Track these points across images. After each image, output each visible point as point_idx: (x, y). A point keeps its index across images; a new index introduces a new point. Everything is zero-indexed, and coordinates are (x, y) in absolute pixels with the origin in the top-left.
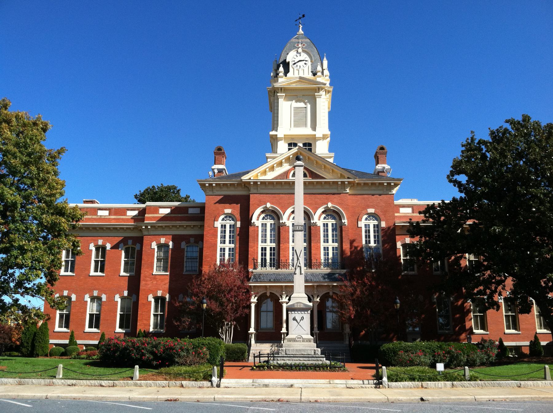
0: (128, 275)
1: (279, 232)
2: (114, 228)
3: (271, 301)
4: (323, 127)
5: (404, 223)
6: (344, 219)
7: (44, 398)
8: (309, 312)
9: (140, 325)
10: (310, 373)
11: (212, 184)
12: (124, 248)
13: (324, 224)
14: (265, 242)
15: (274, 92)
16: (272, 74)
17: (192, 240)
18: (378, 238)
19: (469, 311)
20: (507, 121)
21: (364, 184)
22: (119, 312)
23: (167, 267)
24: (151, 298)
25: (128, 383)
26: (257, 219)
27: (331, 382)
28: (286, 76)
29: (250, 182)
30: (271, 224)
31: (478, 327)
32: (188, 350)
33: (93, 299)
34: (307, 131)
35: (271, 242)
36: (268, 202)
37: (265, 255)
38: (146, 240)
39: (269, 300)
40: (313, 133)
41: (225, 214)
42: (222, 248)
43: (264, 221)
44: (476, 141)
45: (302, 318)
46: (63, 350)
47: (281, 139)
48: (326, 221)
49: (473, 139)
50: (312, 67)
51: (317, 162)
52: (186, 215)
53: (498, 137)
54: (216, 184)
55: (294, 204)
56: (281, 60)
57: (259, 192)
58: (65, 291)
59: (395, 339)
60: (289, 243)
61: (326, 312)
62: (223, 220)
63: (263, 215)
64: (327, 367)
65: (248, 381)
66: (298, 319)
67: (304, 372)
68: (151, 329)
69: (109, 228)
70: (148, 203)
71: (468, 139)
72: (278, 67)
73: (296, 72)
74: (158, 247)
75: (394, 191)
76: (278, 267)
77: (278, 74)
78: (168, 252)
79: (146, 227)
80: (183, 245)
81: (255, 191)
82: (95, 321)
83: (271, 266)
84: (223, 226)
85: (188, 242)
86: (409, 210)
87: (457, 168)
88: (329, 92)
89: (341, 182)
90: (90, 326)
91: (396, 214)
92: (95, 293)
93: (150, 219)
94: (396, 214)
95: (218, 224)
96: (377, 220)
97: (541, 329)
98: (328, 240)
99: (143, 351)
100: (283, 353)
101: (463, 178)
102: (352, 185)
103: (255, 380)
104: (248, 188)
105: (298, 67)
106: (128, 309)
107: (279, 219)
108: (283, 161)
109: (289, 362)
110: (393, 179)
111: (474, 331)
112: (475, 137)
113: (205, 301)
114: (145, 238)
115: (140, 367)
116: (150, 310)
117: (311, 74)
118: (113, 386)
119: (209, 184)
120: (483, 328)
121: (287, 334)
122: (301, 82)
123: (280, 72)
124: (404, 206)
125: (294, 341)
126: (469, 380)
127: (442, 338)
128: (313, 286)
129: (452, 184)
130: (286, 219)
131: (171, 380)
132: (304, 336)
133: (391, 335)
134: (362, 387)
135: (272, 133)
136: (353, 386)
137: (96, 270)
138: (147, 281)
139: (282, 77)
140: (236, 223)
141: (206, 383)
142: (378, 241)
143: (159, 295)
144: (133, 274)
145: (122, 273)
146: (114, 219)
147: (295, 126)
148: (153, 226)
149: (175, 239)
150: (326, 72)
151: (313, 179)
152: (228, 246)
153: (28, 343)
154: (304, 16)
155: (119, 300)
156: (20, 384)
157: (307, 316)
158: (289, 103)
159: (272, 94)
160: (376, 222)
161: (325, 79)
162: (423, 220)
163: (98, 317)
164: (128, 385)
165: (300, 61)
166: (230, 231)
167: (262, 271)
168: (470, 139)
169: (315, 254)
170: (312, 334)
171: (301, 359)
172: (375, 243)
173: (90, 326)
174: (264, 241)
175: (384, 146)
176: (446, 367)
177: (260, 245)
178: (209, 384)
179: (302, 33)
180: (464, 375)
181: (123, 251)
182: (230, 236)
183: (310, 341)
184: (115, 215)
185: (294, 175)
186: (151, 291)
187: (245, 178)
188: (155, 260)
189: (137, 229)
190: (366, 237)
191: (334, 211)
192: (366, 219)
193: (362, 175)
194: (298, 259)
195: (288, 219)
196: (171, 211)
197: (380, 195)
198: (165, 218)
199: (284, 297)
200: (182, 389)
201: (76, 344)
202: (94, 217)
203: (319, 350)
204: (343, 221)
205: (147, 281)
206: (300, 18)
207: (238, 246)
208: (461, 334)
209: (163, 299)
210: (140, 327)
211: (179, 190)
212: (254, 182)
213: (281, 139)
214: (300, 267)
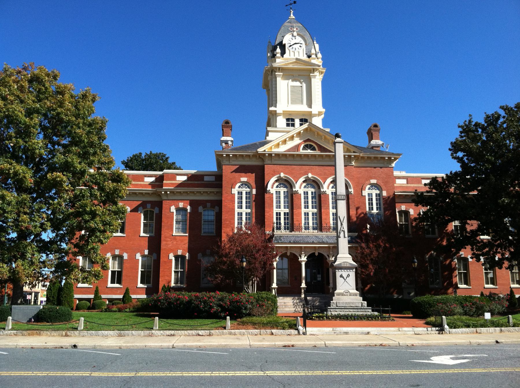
0: (148, 235)
1: (292, 199)
2: (133, 193)
4: (318, 106)
5: (401, 192)
6: (351, 188)
7: (171, 347)
8: (354, 270)
9: (162, 281)
10: (365, 322)
11: (229, 155)
12: (143, 211)
13: (304, 192)
14: (280, 208)
15: (273, 71)
16: (269, 54)
17: (209, 205)
18: (380, 205)
19: (455, 269)
20: (502, 108)
21: (368, 157)
22: (140, 269)
23: (186, 229)
24: (172, 257)
25: (223, 332)
26: (272, 187)
27: (400, 330)
28: (283, 57)
29: (265, 154)
30: (284, 192)
31: (462, 282)
32: (252, 303)
33: (114, 257)
34: (303, 108)
35: (285, 208)
36: (282, 172)
37: (280, 219)
38: (165, 204)
40: (309, 110)
41: (241, 182)
42: (239, 212)
43: (278, 189)
44: (473, 123)
45: (348, 276)
46: (88, 304)
47: (280, 115)
48: (306, 190)
49: (470, 121)
50: (306, 49)
51: (325, 138)
52: (203, 182)
53: (492, 120)
54: (233, 155)
56: (277, 42)
57: (273, 163)
59: (395, 293)
60: (301, 208)
61: (288, 269)
62: (239, 187)
63: (277, 184)
64: (378, 317)
65: (329, 329)
66: (345, 275)
67: (358, 321)
68: (173, 284)
69: (136, 193)
70: (166, 171)
71: (466, 121)
72: (275, 48)
73: (292, 54)
74: (176, 211)
75: (393, 165)
76: (292, 230)
77: (276, 55)
78: (186, 215)
79: (166, 192)
80: (200, 209)
81: (269, 162)
82: (117, 277)
83: (285, 229)
84: (240, 193)
85: (205, 207)
86: (404, 181)
87: (455, 147)
88: (322, 73)
89: (348, 155)
90: (113, 282)
92: (117, 252)
93: (168, 185)
95: (235, 191)
96: (379, 190)
97: (514, 284)
98: (280, 206)
99: (211, 304)
100: (335, 306)
101: (460, 154)
102: (357, 158)
103: (334, 328)
105: (294, 49)
106: (149, 267)
107: (319, 188)
108: (295, 135)
109: (342, 313)
110: (393, 154)
111: (459, 286)
112: (472, 120)
113: (244, 260)
114: (164, 203)
116: (171, 267)
117: (306, 56)
118: (210, 335)
119: (226, 155)
120: (466, 283)
122: (297, 63)
123: (277, 53)
124: (399, 178)
125: (343, 295)
126: (513, 326)
127: (433, 292)
128: (329, 247)
129: (456, 161)
130: (327, 188)
131: (260, 329)
132: (351, 291)
133: (392, 290)
134: (428, 334)
135: (271, 109)
136: (420, 333)
138: (167, 241)
139: (279, 58)
140: (252, 191)
141: (293, 332)
142: (380, 208)
143: (179, 254)
144: (153, 234)
145: (142, 234)
148: (172, 192)
149: (192, 203)
150: (320, 55)
152: (245, 210)
153: (53, 297)
154: (295, 2)
155: (140, 258)
156: (120, 335)
157: (352, 274)
158: (286, 82)
159: (270, 73)
160: (378, 192)
161: (318, 61)
162: (427, 191)
163: (120, 273)
164: (223, 334)
165: (296, 44)
166: (246, 197)
168: (468, 121)
169: (326, 219)
170: (357, 289)
171: (351, 310)
172: (377, 210)
173: (113, 282)
174: (279, 207)
175: (378, 124)
176: (492, 315)
177: (275, 210)
178: (296, 332)
179: (294, 17)
180: (509, 322)
181: (142, 214)
182: (246, 202)
183: (356, 295)
186: (171, 251)
187: (261, 150)
188: (175, 223)
189: (154, 194)
190: (369, 205)
191: (314, 181)
192: (369, 189)
193: (361, 149)
194: (342, 224)
195: (300, 188)
196: (188, 178)
197: (381, 168)
198: (182, 185)
199: (303, 256)
200: (272, 336)
201: (101, 299)
202: (142, 183)
203: (366, 302)
204: (350, 190)
205: (167, 241)
206: (291, 4)
207: (254, 211)
208: (448, 289)
209: (183, 257)
210: (162, 283)
211: (167, 158)
212: (269, 154)
213: (280, 115)
214: (344, 231)
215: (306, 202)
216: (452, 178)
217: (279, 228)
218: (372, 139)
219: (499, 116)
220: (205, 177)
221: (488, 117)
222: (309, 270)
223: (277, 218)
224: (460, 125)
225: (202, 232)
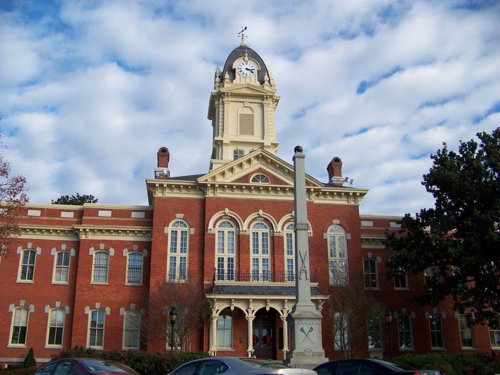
17: (135, 247)
20: (478, 135)
29: (206, 184)
40: (262, 141)
42: (176, 258)
49: (444, 150)
66: (306, 329)
71: (439, 150)
85: (97, 248)
95: (168, 230)
104: (204, 192)
129: (431, 194)
137: (23, 277)
146: (46, 220)
147: (241, 133)
151: (275, 184)
154: (246, 28)
157: (319, 322)
167: (253, 283)
168: (441, 150)
177: (217, 254)
184: (48, 215)
194: (303, 262)
215: (256, 245)
216: (426, 214)
217: (221, 277)
218: (333, 175)
219: (476, 144)
220: (133, 213)
221: (463, 145)
222: (257, 331)
223: (219, 265)
224: (433, 155)
225: (127, 281)
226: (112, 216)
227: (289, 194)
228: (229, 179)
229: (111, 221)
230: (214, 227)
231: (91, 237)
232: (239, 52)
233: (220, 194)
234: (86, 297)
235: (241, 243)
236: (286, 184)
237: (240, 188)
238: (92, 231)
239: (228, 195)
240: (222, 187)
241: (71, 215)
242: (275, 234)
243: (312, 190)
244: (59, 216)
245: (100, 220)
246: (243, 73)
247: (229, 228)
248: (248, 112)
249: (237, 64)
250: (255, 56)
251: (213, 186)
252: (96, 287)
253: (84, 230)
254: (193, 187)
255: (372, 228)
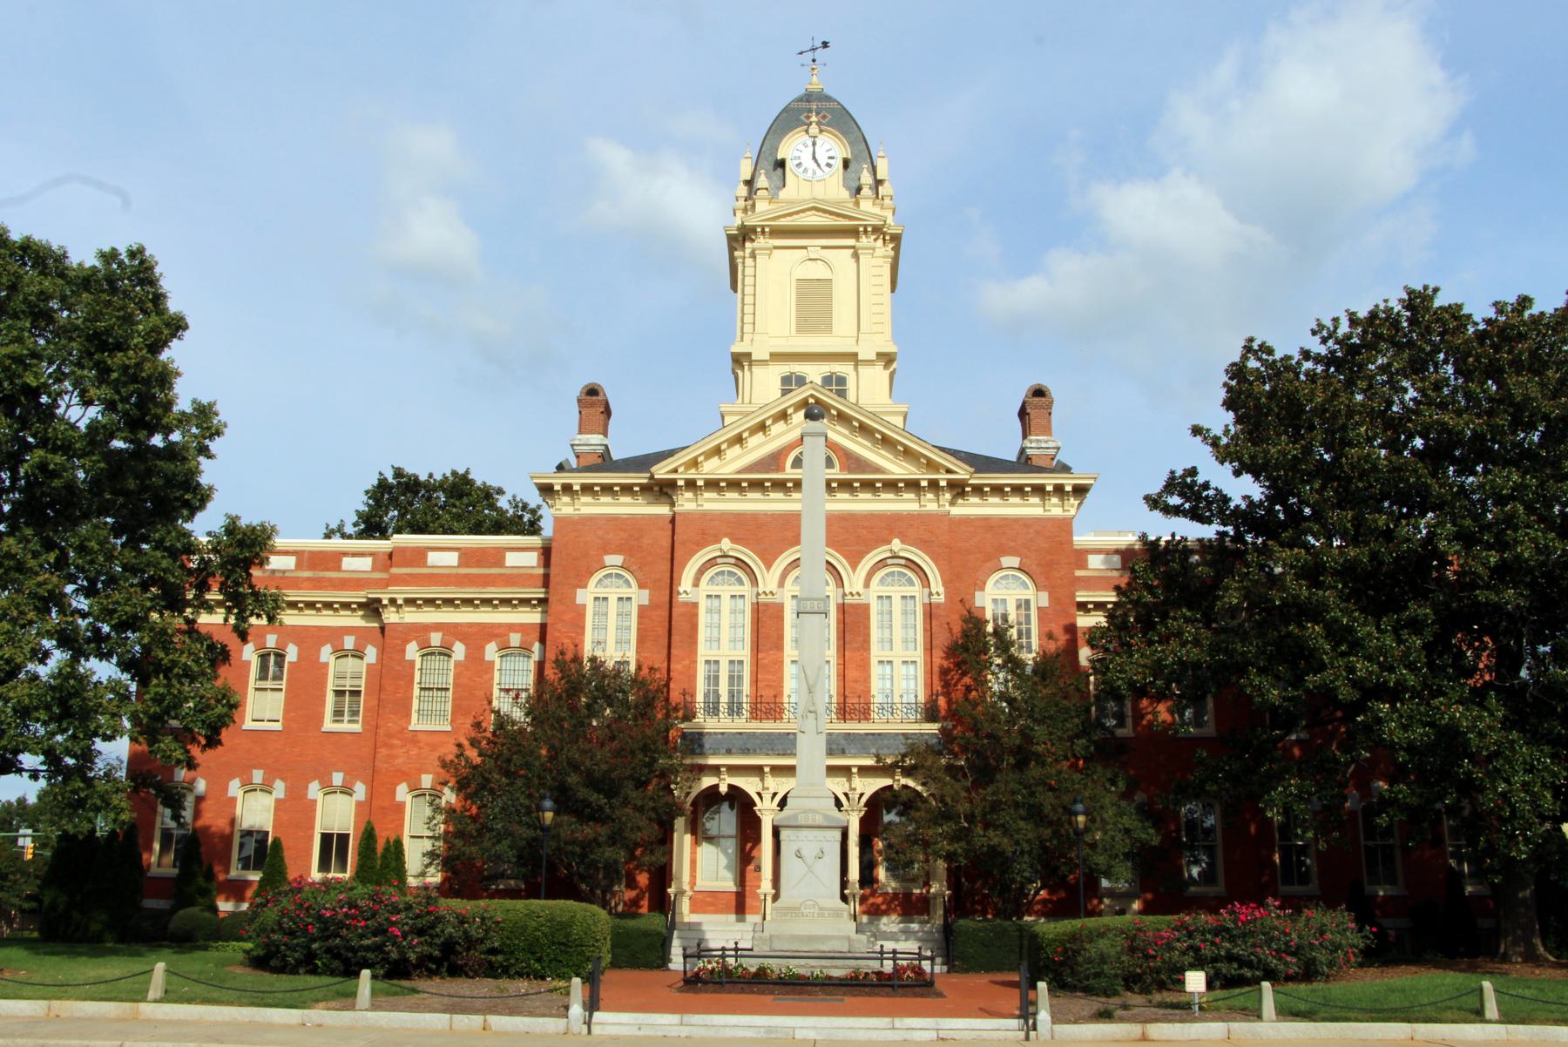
3: (732, 807)
36: (726, 535)
39: (725, 807)
55: (796, 541)
58: (424, 777)
80: (491, 651)
91: (1079, 573)
94: (1079, 573)
115: (374, 977)
121: (776, 897)
146: (308, 579)
151: (850, 472)
154: (825, 45)
177: (704, 651)
184: (312, 567)
185: (798, 463)
217: (713, 709)
226: (374, 569)
227: (906, 496)
228: (731, 464)
229: (457, 575)
230: (696, 584)
231: (411, 616)
232: (800, 111)
233: (711, 503)
234: (400, 761)
235: (766, 625)
236: (878, 470)
237: (757, 485)
238: (410, 602)
239: (732, 503)
240: (712, 485)
241: (365, 564)
242: (849, 600)
243: (943, 483)
244: (338, 568)
245: (1089, 578)
246: (805, 171)
247: (1018, 591)
248: (817, 271)
249: (793, 147)
250: (840, 120)
251: (691, 484)
252: (421, 736)
253: (393, 601)
254: (645, 489)
255: (454, 571)
